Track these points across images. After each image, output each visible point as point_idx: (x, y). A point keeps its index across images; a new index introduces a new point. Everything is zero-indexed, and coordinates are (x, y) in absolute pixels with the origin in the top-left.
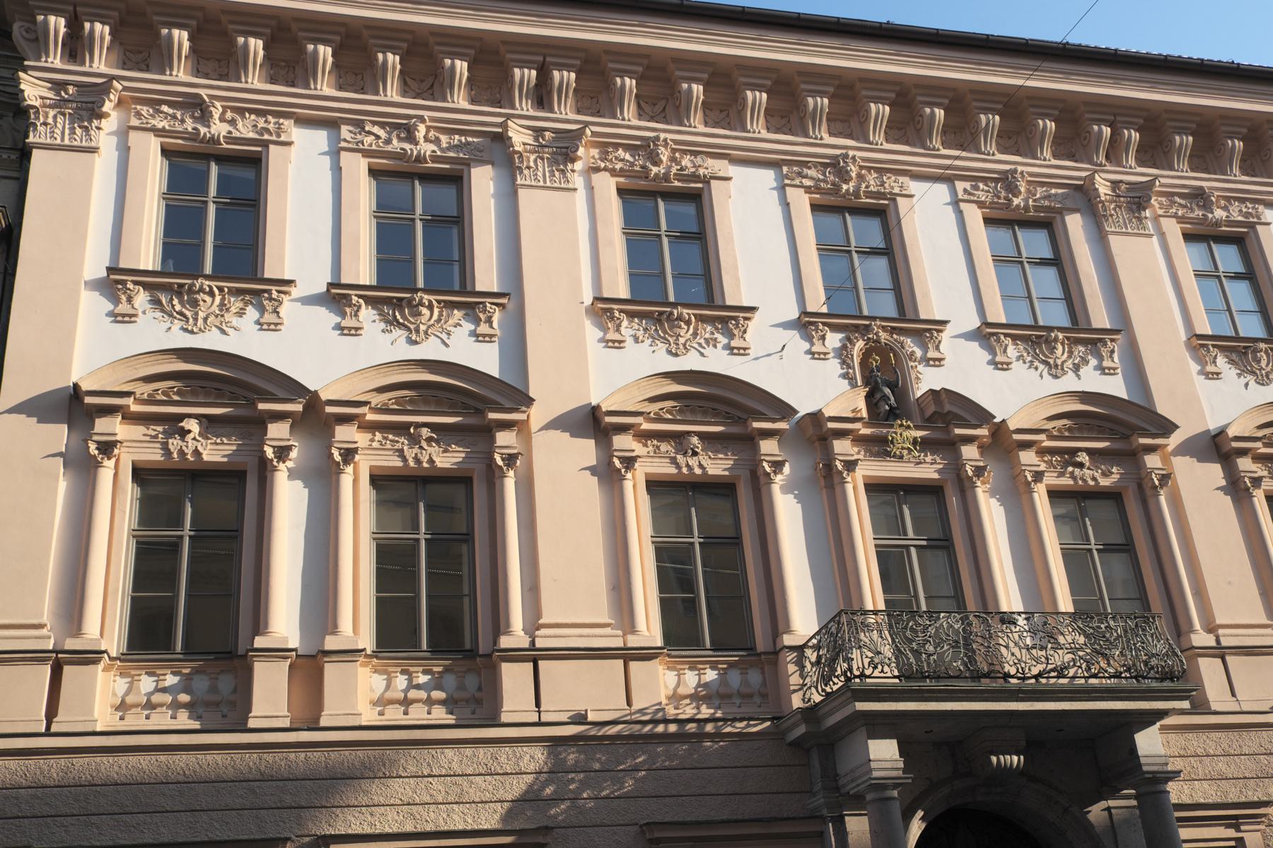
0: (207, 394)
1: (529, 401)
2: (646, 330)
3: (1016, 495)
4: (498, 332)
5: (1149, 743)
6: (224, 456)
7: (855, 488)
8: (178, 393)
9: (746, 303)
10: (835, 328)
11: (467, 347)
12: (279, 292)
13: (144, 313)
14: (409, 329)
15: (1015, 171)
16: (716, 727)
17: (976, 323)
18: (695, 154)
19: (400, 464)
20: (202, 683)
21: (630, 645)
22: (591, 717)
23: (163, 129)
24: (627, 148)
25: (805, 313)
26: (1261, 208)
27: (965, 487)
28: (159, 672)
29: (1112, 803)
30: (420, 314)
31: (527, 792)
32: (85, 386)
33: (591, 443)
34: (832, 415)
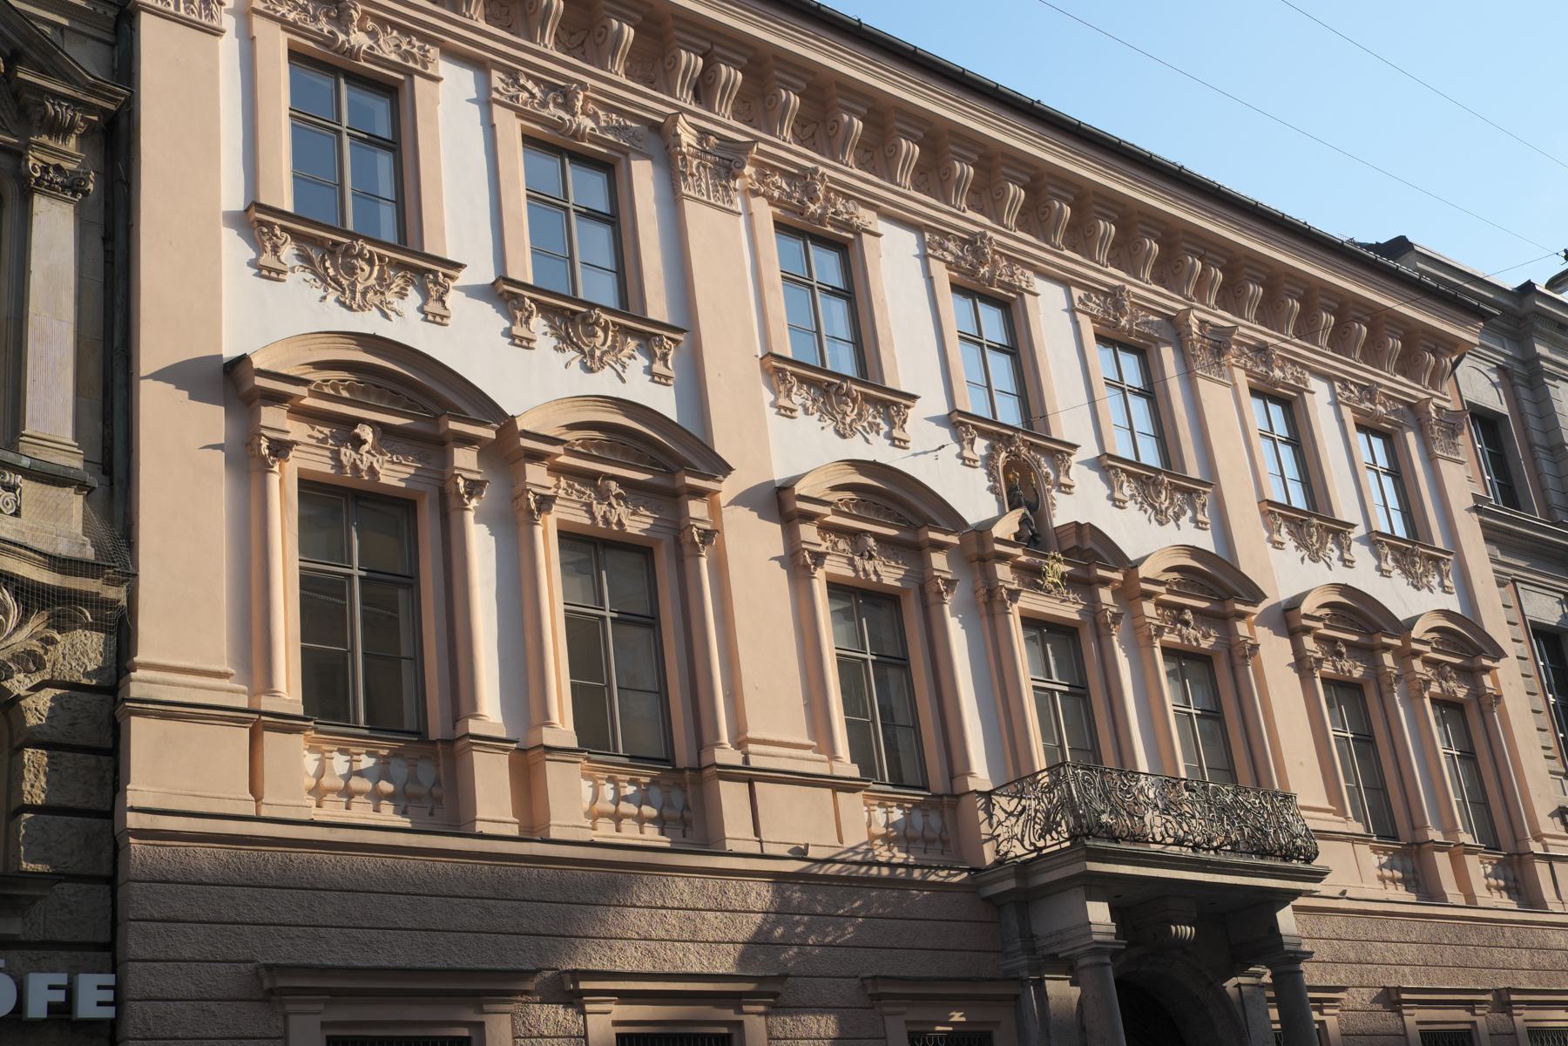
0: (380, 397)
1: (726, 469)
2: (814, 400)
3: (514, 524)
4: (672, 374)
5: (1286, 919)
6: (401, 480)
7: (545, 533)
8: (348, 389)
9: (904, 388)
10: (984, 434)
11: (639, 383)
12: (445, 275)
13: (293, 270)
14: (582, 352)
15: (1123, 288)
16: (923, 874)
17: (944, 411)
18: (848, 197)
19: (588, 522)
20: (400, 769)
21: (836, 773)
22: (813, 853)
23: (294, 24)
24: (784, 174)
25: (255, 205)
26: (434, 52)
27: (1101, 634)
28: (354, 750)
29: (1242, 980)
30: (594, 335)
31: (757, 934)
32: (258, 362)
33: (778, 527)
34: (263, 367)
